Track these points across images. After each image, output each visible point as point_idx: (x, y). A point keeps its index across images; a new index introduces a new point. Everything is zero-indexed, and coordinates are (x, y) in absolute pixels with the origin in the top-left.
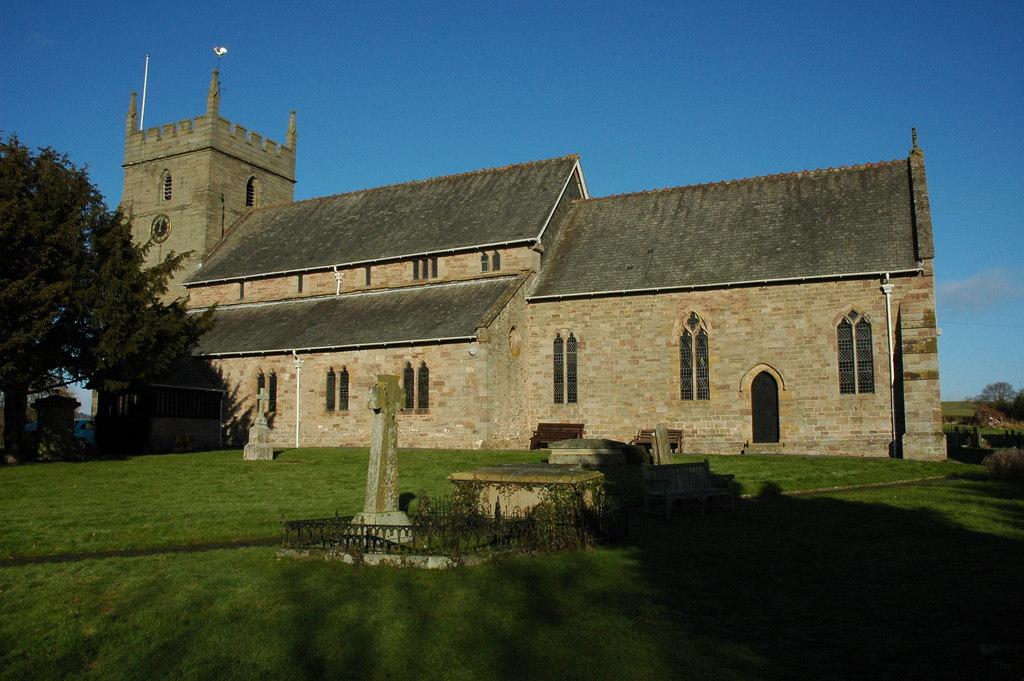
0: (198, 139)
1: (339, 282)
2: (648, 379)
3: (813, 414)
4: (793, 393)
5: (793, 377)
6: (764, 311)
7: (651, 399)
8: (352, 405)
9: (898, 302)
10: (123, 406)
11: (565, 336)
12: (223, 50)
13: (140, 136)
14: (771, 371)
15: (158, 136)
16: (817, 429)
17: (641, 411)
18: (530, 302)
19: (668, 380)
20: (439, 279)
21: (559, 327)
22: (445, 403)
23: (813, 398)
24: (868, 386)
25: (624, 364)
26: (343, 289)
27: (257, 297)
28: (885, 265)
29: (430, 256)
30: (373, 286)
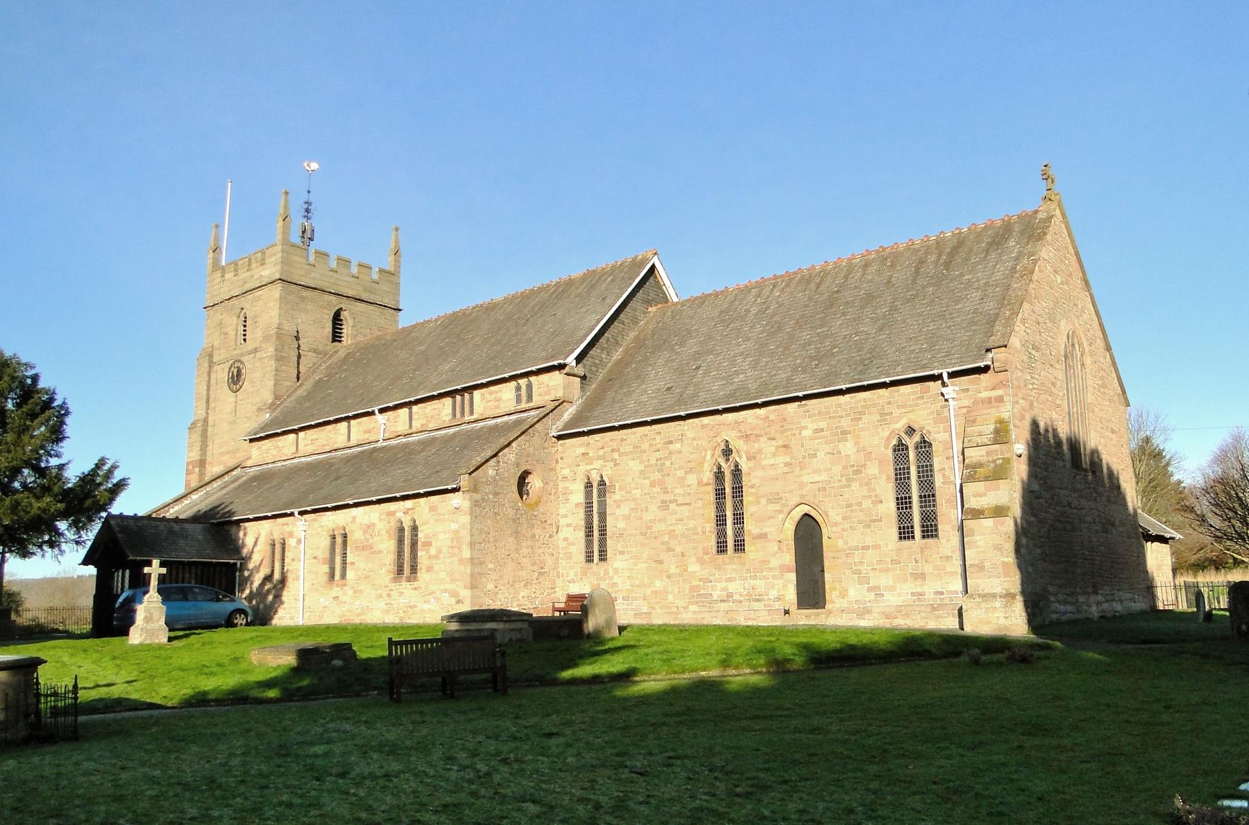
0: (270, 271)
1: (383, 427)
2: (679, 528)
3: (863, 568)
5: (839, 519)
6: (805, 433)
7: (683, 555)
8: (350, 574)
9: (964, 411)
10: (177, 574)
12: (314, 166)
13: (219, 273)
14: (813, 513)
15: (235, 271)
16: (869, 590)
17: (673, 570)
18: (560, 438)
19: (700, 530)
20: (475, 416)
21: (589, 467)
22: (432, 567)
23: (863, 548)
24: (930, 531)
25: (654, 511)
26: (387, 436)
27: (310, 449)
28: (372, 402)
29: (465, 389)
30: (414, 430)
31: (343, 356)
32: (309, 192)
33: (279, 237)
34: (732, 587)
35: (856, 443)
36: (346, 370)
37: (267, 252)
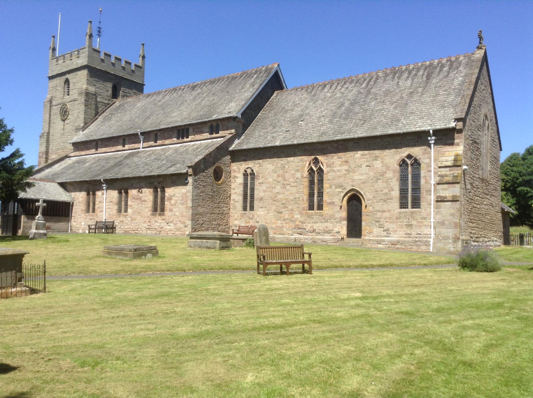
0: (83, 61)
4: (371, 208)
7: (292, 210)
8: (130, 210)
11: (249, 171)
13: (55, 60)
16: (384, 231)
19: (301, 198)
25: (278, 188)
31: (118, 105)
32: (100, 22)
33: (87, 43)
34: (315, 226)
35: (382, 162)
36: (120, 113)
37: (80, 51)
